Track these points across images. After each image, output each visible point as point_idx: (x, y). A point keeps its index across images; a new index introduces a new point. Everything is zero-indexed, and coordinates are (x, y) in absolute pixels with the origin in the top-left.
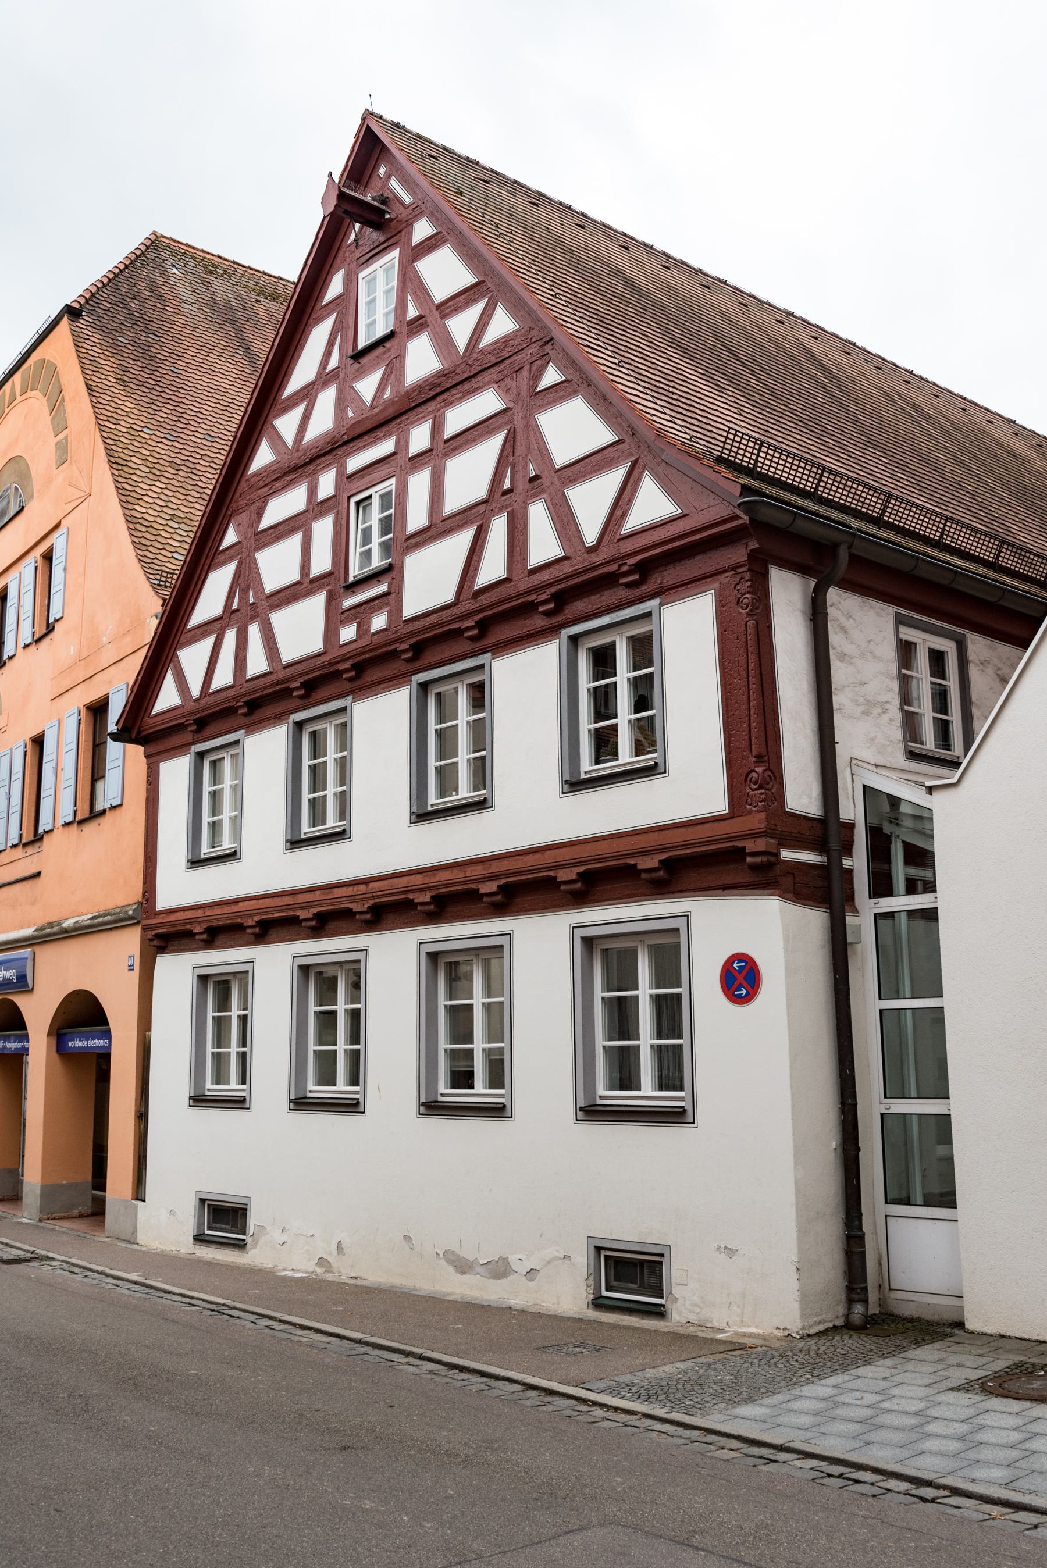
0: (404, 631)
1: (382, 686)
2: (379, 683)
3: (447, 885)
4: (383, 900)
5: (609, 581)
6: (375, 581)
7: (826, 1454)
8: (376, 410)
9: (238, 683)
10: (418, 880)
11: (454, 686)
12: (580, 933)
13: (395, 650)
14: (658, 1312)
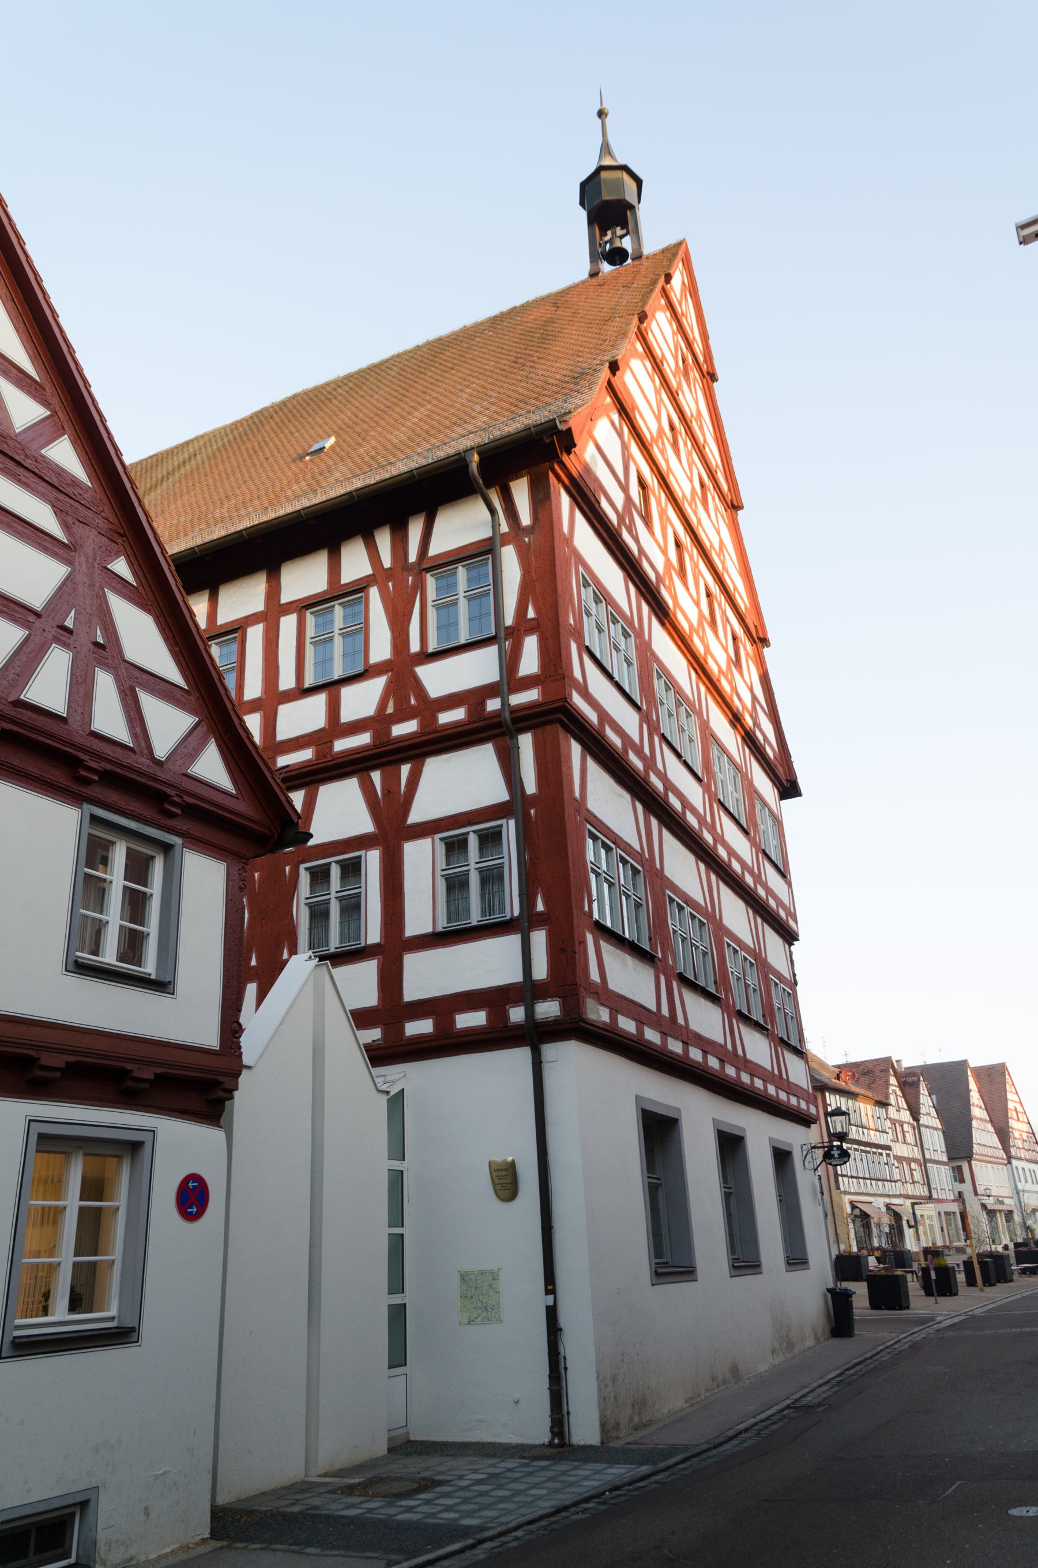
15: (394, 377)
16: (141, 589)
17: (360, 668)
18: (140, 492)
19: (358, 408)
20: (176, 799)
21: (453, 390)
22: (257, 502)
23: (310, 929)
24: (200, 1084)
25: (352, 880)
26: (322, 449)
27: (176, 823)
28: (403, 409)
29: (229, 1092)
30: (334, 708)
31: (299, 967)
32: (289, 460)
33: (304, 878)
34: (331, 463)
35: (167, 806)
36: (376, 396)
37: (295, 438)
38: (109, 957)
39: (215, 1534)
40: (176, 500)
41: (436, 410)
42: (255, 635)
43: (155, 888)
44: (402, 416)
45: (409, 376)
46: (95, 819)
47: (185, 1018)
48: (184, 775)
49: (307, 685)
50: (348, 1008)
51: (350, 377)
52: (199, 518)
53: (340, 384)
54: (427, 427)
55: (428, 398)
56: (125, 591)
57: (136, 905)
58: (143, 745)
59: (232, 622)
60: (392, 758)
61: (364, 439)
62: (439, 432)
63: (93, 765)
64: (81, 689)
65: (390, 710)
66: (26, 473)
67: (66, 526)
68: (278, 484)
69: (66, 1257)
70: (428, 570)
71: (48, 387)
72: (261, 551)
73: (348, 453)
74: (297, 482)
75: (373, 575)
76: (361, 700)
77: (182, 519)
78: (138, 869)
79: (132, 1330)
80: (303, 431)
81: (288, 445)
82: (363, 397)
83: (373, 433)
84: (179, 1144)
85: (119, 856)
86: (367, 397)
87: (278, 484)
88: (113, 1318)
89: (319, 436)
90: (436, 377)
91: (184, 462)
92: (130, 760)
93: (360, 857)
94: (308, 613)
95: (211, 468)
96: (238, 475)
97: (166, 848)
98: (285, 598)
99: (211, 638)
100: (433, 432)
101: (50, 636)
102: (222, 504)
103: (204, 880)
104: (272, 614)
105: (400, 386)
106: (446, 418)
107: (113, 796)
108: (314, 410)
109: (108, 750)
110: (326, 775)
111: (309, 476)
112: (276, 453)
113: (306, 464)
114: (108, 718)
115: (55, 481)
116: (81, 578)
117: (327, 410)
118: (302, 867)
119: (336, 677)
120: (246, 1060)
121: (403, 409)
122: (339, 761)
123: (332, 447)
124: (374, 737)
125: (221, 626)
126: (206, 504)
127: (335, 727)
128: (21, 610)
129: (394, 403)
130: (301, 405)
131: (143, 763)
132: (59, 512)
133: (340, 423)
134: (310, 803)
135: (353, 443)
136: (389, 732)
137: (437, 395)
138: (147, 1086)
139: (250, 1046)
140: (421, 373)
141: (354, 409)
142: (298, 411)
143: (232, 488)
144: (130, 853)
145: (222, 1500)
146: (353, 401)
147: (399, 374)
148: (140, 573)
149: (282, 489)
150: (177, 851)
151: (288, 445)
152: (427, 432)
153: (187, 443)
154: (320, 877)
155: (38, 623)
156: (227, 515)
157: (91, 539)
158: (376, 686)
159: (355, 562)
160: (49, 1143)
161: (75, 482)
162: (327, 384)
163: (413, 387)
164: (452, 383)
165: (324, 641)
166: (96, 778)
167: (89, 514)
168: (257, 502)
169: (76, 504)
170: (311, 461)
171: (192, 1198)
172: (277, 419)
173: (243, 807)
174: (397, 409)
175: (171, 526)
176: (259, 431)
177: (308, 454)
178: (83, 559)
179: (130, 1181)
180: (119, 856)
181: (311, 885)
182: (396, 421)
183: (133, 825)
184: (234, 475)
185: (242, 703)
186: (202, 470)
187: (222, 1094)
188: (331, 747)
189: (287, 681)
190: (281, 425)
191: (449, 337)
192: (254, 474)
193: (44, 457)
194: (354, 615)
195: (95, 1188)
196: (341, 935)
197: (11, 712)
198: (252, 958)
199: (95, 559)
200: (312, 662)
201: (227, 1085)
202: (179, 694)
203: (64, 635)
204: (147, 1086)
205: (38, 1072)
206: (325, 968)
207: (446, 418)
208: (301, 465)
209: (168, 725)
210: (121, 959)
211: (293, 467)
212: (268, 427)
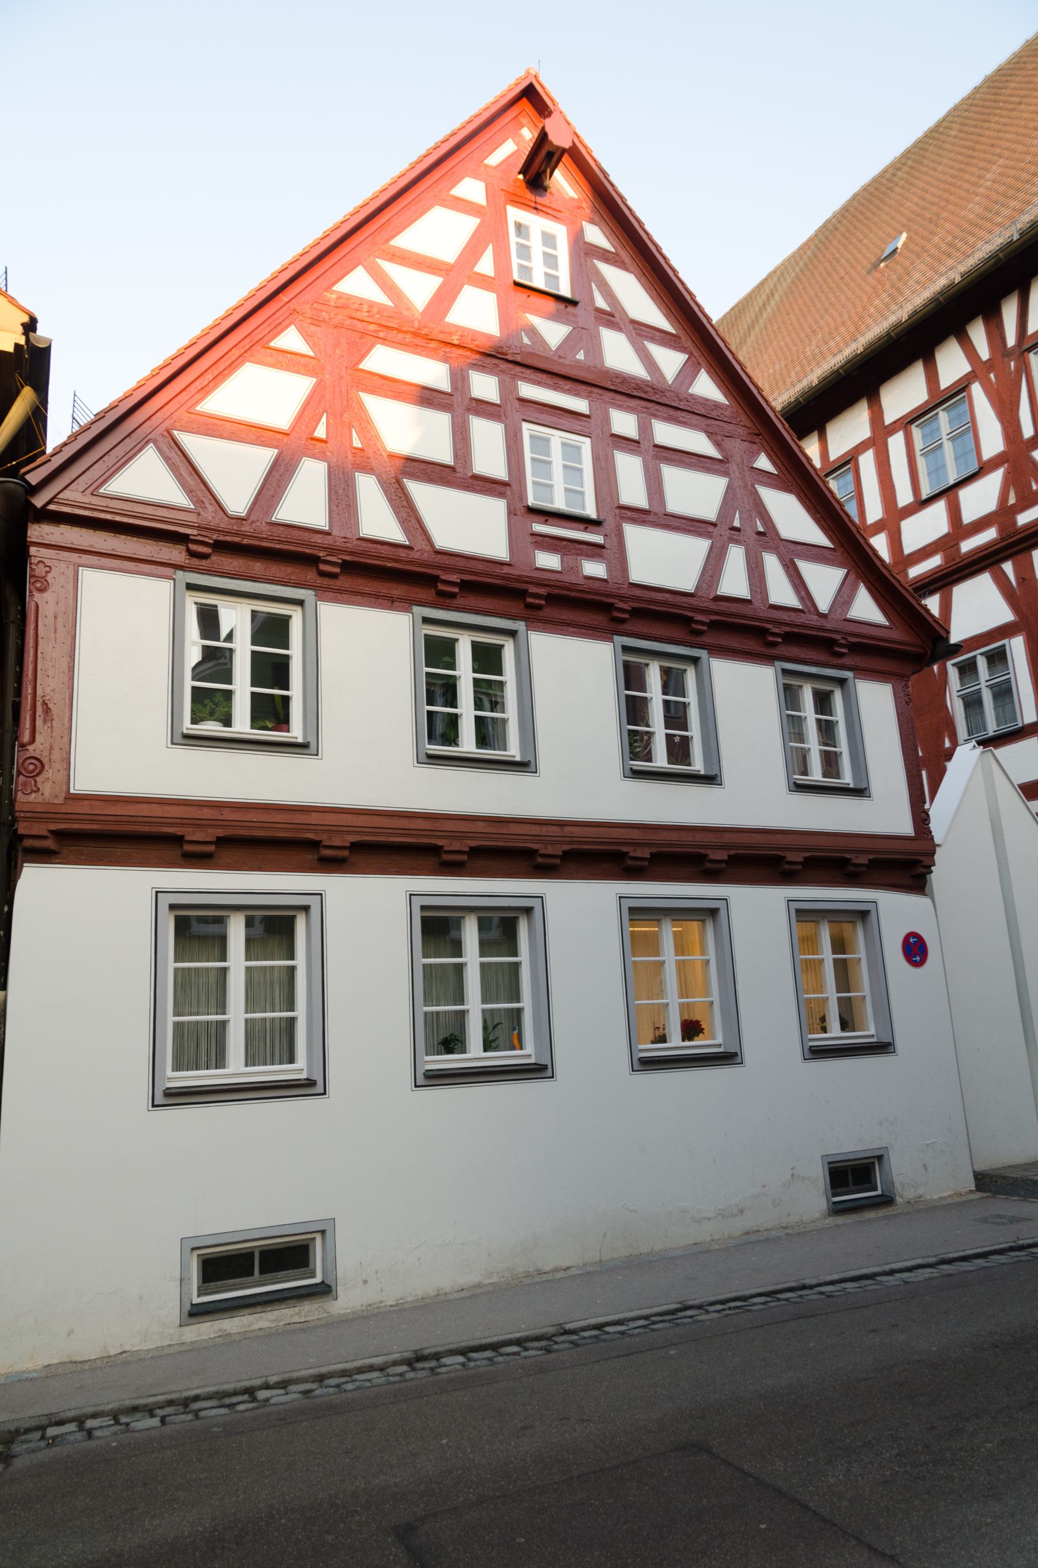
0: (625, 591)
1: (571, 629)
2: (569, 625)
3: (670, 845)
4: (585, 847)
5: (310, 561)
6: (582, 526)
7: (484, 1341)
8: (561, 360)
9: (253, 518)
10: (635, 835)
11: (683, 667)
12: (794, 906)
13: (438, 577)
14: (886, 1201)
15: (955, 137)
16: (781, 475)
17: (974, 467)
18: (733, 349)
19: (923, 189)
20: (843, 641)
21: (1024, 131)
22: (842, 330)
23: (966, 718)
24: (905, 864)
25: (1000, 667)
26: (895, 251)
27: (846, 661)
28: (973, 174)
29: (928, 869)
30: (954, 512)
31: (965, 760)
32: (864, 273)
33: (953, 674)
34: (907, 263)
35: (837, 649)
36: (940, 168)
37: (865, 246)
38: (816, 775)
39: (979, 1188)
40: (766, 349)
41: (1011, 163)
42: (867, 462)
43: (839, 714)
44: (973, 184)
45: (972, 129)
46: (785, 672)
47: (884, 814)
48: (845, 620)
49: (924, 497)
50: (1016, 783)
51: (907, 154)
52: (792, 362)
53: (898, 165)
54: (1002, 189)
55: (998, 151)
56: (770, 481)
57: (827, 730)
58: (809, 604)
59: (844, 455)
60: (1022, 546)
61: (937, 225)
62: (1018, 190)
63: (776, 630)
64: (341, 497)
65: (1012, 500)
67: (718, 445)
68: (858, 303)
69: (831, 993)
70: (1029, 350)
71: (682, 334)
72: (859, 381)
73: (923, 247)
74: (878, 296)
75: (973, 371)
76: (981, 499)
77: (777, 367)
78: (823, 702)
79: (889, 1044)
80: (871, 236)
81: (859, 256)
82: (926, 174)
83: (945, 214)
84: (896, 911)
86: (931, 172)
87: (858, 303)
88: (873, 1036)
89: (889, 235)
90: (1004, 120)
91: (764, 305)
92: (802, 619)
93: (1004, 645)
94: (913, 427)
95: (790, 304)
96: (818, 305)
97: (842, 682)
98: (888, 420)
99: (827, 475)
100: (1011, 192)
101: (725, 538)
102: (810, 341)
103: (876, 702)
105: (963, 147)
106: (1022, 170)
107: (795, 651)
108: (877, 207)
109: (784, 616)
110: (957, 576)
111: (888, 285)
112: (849, 269)
113: (882, 272)
114: (781, 592)
116: (738, 483)
117: (891, 202)
118: (949, 664)
119: (952, 482)
120: (937, 841)
121: (973, 174)
122: (968, 560)
123: (905, 245)
124: (1000, 531)
125: (834, 461)
126: (795, 345)
127: (959, 529)
128: (703, 525)
129: (962, 170)
130: (863, 205)
131: (813, 620)
132: (710, 435)
133: (907, 212)
134: (946, 606)
135: (926, 233)
136: (1015, 522)
137: (1008, 145)
138: (864, 869)
139: (938, 827)
140: (984, 121)
141: (919, 192)
142: (861, 213)
143: (815, 320)
145: (980, 1167)
146: (916, 182)
147: (961, 131)
148: (778, 461)
149: (864, 308)
150: (850, 682)
151: (859, 256)
152: (1005, 195)
153: (762, 283)
154: (968, 670)
155: (716, 531)
156: (817, 351)
157: (737, 447)
158: (994, 481)
159: (952, 363)
160: (804, 915)
161: (717, 405)
162: (885, 171)
163: (978, 142)
164: (1023, 123)
165: (934, 449)
166: (780, 640)
167: (731, 427)
168: (842, 330)
169: (721, 423)
170: (887, 266)
171: (915, 949)
172: (842, 229)
173: (895, 635)
174: (967, 176)
175: (769, 376)
176: (827, 249)
177: (882, 261)
178: (735, 467)
179: (865, 938)
181: (961, 679)
182: (968, 191)
184: (814, 306)
185: (867, 528)
186: (782, 310)
187: (923, 870)
188: (958, 550)
189: (904, 497)
190: (848, 235)
191: (1009, 62)
192: (833, 299)
193: (691, 395)
194: (959, 416)
195: (839, 945)
196: (997, 719)
197: (713, 606)
198: (926, 759)
199: (743, 464)
200: (926, 472)
201: (926, 862)
202: (827, 553)
203: (315, 447)
205: (787, 867)
206: (989, 754)
207: (1022, 170)
208: (877, 275)
209: (825, 581)
210: (824, 776)
211: (870, 280)
212: (835, 242)
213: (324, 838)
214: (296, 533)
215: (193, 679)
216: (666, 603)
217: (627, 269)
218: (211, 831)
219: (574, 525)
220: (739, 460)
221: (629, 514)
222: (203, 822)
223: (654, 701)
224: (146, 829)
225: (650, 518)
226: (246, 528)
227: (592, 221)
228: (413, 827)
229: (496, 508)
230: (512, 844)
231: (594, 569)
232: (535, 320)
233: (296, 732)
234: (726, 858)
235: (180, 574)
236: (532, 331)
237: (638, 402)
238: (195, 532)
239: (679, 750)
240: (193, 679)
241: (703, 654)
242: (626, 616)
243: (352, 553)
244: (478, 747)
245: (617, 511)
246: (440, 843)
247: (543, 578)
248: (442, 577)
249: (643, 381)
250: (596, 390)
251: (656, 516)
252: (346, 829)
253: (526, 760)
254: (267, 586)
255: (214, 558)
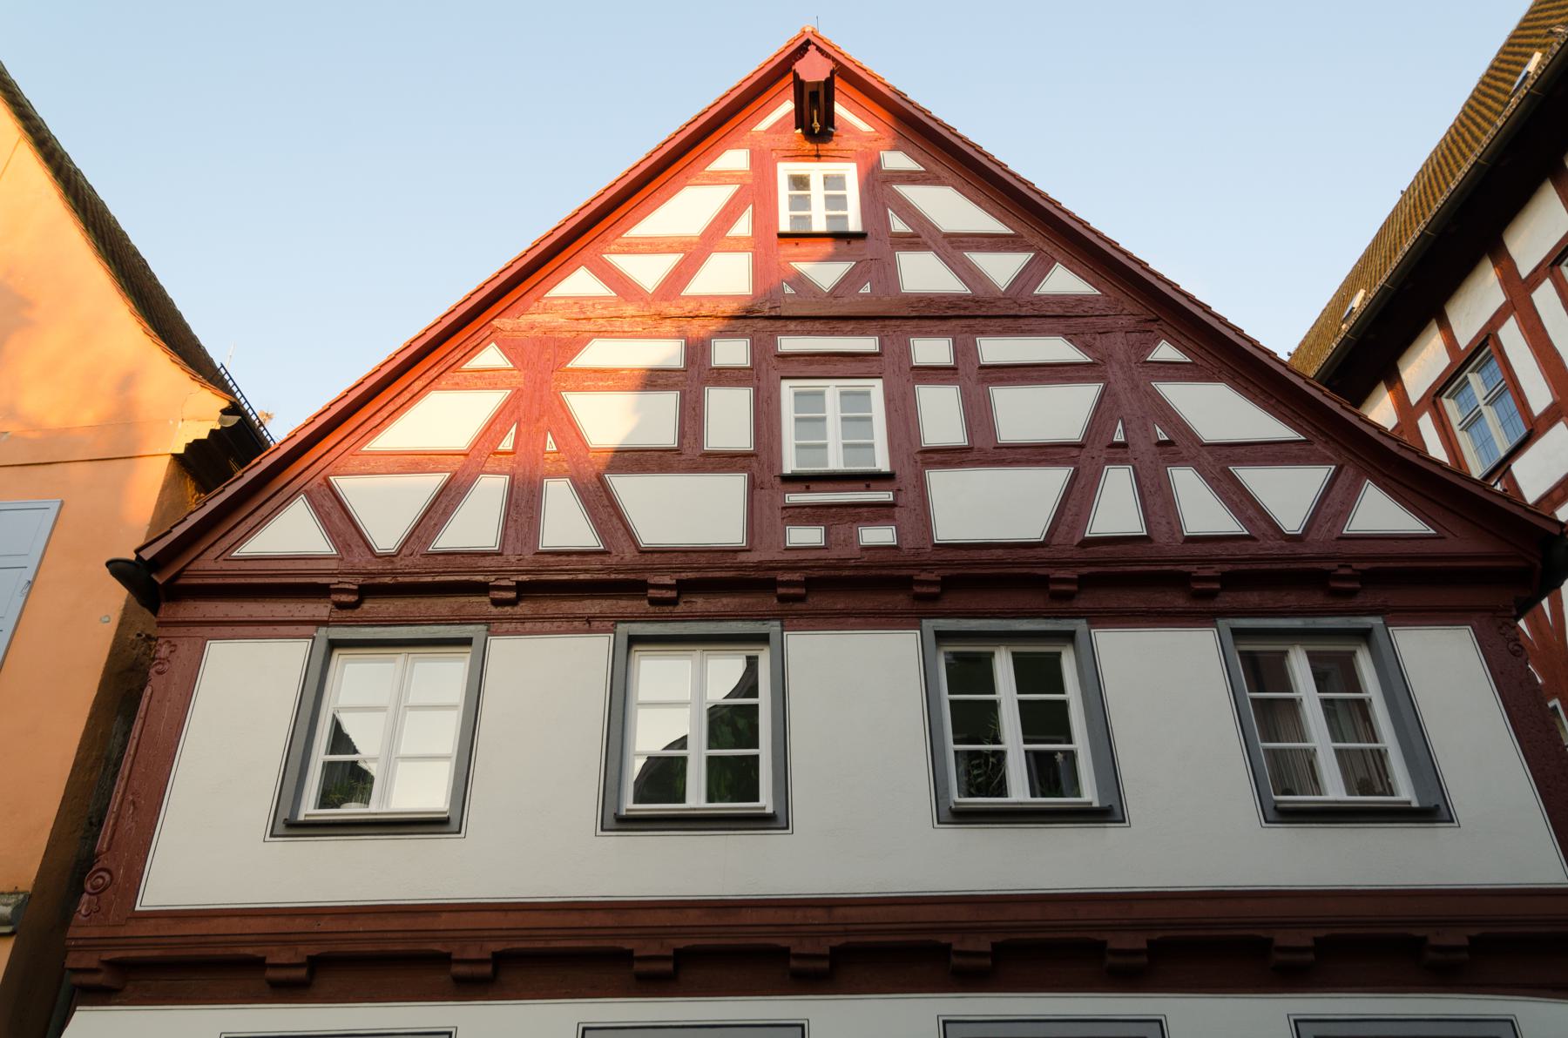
1: (852, 620)
6: (863, 485)
20: (1342, 571)
38: (1334, 790)
42: (1511, 335)
43: (1371, 688)
46: (1238, 633)
48: (1339, 539)
59: (1477, 336)
64: (1156, 498)
66: (1026, 321)
67: (1084, 347)
85: (1299, 666)
92: (1252, 549)
97: (1365, 636)
98: (1525, 270)
101: (1102, 460)
104: (1518, 301)
107: (1253, 598)
114: (1201, 511)
115: (1059, 311)
131: (1271, 546)
132: (1071, 337)
144: (1313, 657)
148: (1190, 345)
150: (1379, 635)
155: (1084, 454)
161: (1080, 300)
166: (1217, 586)
178: (1116, 367)
180: (1299, 666)
183: (1297, 623)
202: (1295, 449)
203: (1118, 453)
204: (1144, 959)
210: (710, 799)
213: (456, 950)
214: (974, 555)
215: (956, 742)
216: (999, 563)
217: (943, 184)
218: (302, 949)
219: (848, 486)
220: (1122, 357)
221: (937, 457)
222: (292, 937)
223: (1306, 703)
224: (220, 951)
225: (971, 456)
226: (399, 564)
227: (894, 148)
228: (586, 924)
229: (734, 486)
230: (742, 941)
231: (878, 535)
232: (803, 267)
233: (766, 801)
234: (1144, 946)
235: (323, 631)
236: (800, 281)
237: (954, 322)
238: (335, 580)
239: (1050, 773)
240: (956, 742)
241: (1080, 626)
242: (1074, 588)
243: (527, 572)
244: (1350, 793)
245: (919, 457)
246: (627, 945)
247: (801, 560)
248: (651, 581)
249: (960, 297)
250: (893, 322)
251: (983, 451)
252: (486, 933)
253: (1106, 804)
254: (733, 624)
255: (810, 600)
